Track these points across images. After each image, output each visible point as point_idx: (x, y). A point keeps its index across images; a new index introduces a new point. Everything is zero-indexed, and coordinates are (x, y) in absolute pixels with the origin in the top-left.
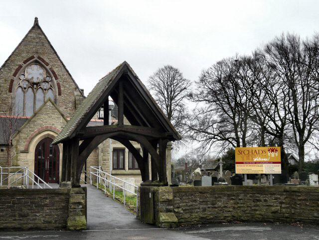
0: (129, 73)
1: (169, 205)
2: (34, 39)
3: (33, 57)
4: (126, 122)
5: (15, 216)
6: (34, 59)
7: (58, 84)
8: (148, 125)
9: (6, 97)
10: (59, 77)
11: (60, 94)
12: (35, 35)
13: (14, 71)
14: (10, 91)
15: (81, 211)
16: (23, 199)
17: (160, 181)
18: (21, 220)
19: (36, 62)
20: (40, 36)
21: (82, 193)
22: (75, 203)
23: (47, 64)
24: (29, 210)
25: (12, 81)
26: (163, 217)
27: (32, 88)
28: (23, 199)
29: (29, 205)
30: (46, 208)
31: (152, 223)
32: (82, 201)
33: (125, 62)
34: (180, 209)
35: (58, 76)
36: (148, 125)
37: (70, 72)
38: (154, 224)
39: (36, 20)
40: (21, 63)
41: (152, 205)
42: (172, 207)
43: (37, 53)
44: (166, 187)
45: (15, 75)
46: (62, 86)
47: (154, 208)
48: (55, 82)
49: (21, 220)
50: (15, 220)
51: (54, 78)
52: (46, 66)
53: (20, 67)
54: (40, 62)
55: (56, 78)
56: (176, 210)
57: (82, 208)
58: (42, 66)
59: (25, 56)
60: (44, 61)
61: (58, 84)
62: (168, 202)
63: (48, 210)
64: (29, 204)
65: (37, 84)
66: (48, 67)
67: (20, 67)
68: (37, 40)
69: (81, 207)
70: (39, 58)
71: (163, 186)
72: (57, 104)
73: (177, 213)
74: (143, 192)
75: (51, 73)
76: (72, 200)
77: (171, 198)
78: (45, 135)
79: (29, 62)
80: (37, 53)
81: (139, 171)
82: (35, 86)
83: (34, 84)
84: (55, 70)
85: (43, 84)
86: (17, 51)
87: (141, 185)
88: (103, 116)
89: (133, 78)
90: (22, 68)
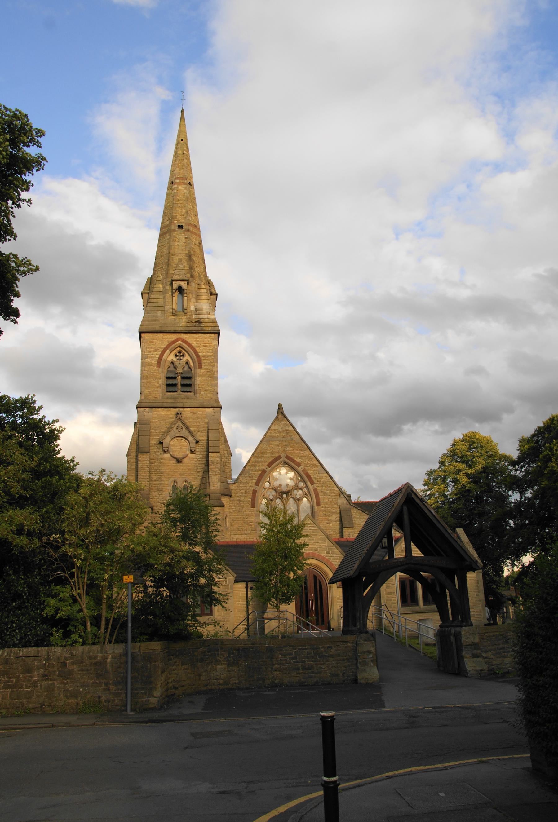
0: (413, 496)
1: (475, 649)
2: (279, 432)
3: (279, 458)
4: (416, 552)
5: (298, 669)
6: (281, 460)
7: (315, 490)
8: (442, 553)
9: (249, 515)
10: (315, 481)
11: (318, 505)
12: (280, 428)
13: (256, 479)
14: (253, 506)
15: (372, 661)
16: (305, 649)
17: (462, 621)
18: (305, 673)
19: (285, 464)
20: (287, 428)
21: (371, 641)
22: (364, 652)
23: (299, 465)
24: (313, 661)
25: (255, 492)
26: (471, 665)
27: (281, 498)
28: (305, 649)
29: (313, 656)
30: (331, 659)
31: (217, 335)
32: (372, 649)
33: (408, 483)
34: (490, 653)
35: (314, 480)
36: (442, 553)
37: (330, 473)
38: (459, 672)
39: (280, 408)
40: (265, 467)
41: (455, 651)
42: (479, 651)
43: (284, 451)
44: (470, 627)
45: (257, 484)
46: (320, 493)
47: (457, 654)
48: (311, 487)
49: (305, 673)
50: (299, 673)
51: (309, 483)
52: (296, 467)
53: (264, 471)
54: (290, 464)
55: (312, 483)
56: (484, 655)
57: (372, 657)
58: (293, 469)
59: (269, 457)
60: (293, 461)
61: (315, 490)
62: (475, 646)
63: (334, 661)
64: (313, 655)
65: (287, 493)
66: (299, 469)
67: (264, 471)
68: (284, 434)
69: (371, 656)
70: (287, 457)
71: (465, 626)
72: (316, 518)
73: (486, 658)
74: (442, 635)
75: (304, 477)
76: (360, 649)
77: (477, 640)
78: (321, 568)
79: (275, 464)
80: (284, 451)
81: (434, 607)
82: (285, 496)
83: (283, 493)
84: (310, 472)
85: (295, 492)
86: (258, 451)
87: (440, 626)
88: (386, 544)
89: (418, 501)
90: (266, 473)
